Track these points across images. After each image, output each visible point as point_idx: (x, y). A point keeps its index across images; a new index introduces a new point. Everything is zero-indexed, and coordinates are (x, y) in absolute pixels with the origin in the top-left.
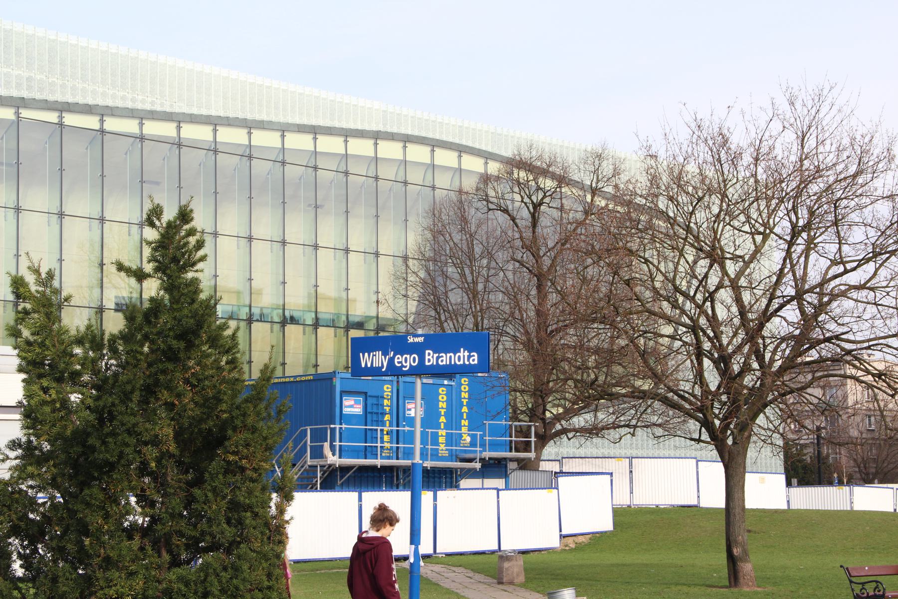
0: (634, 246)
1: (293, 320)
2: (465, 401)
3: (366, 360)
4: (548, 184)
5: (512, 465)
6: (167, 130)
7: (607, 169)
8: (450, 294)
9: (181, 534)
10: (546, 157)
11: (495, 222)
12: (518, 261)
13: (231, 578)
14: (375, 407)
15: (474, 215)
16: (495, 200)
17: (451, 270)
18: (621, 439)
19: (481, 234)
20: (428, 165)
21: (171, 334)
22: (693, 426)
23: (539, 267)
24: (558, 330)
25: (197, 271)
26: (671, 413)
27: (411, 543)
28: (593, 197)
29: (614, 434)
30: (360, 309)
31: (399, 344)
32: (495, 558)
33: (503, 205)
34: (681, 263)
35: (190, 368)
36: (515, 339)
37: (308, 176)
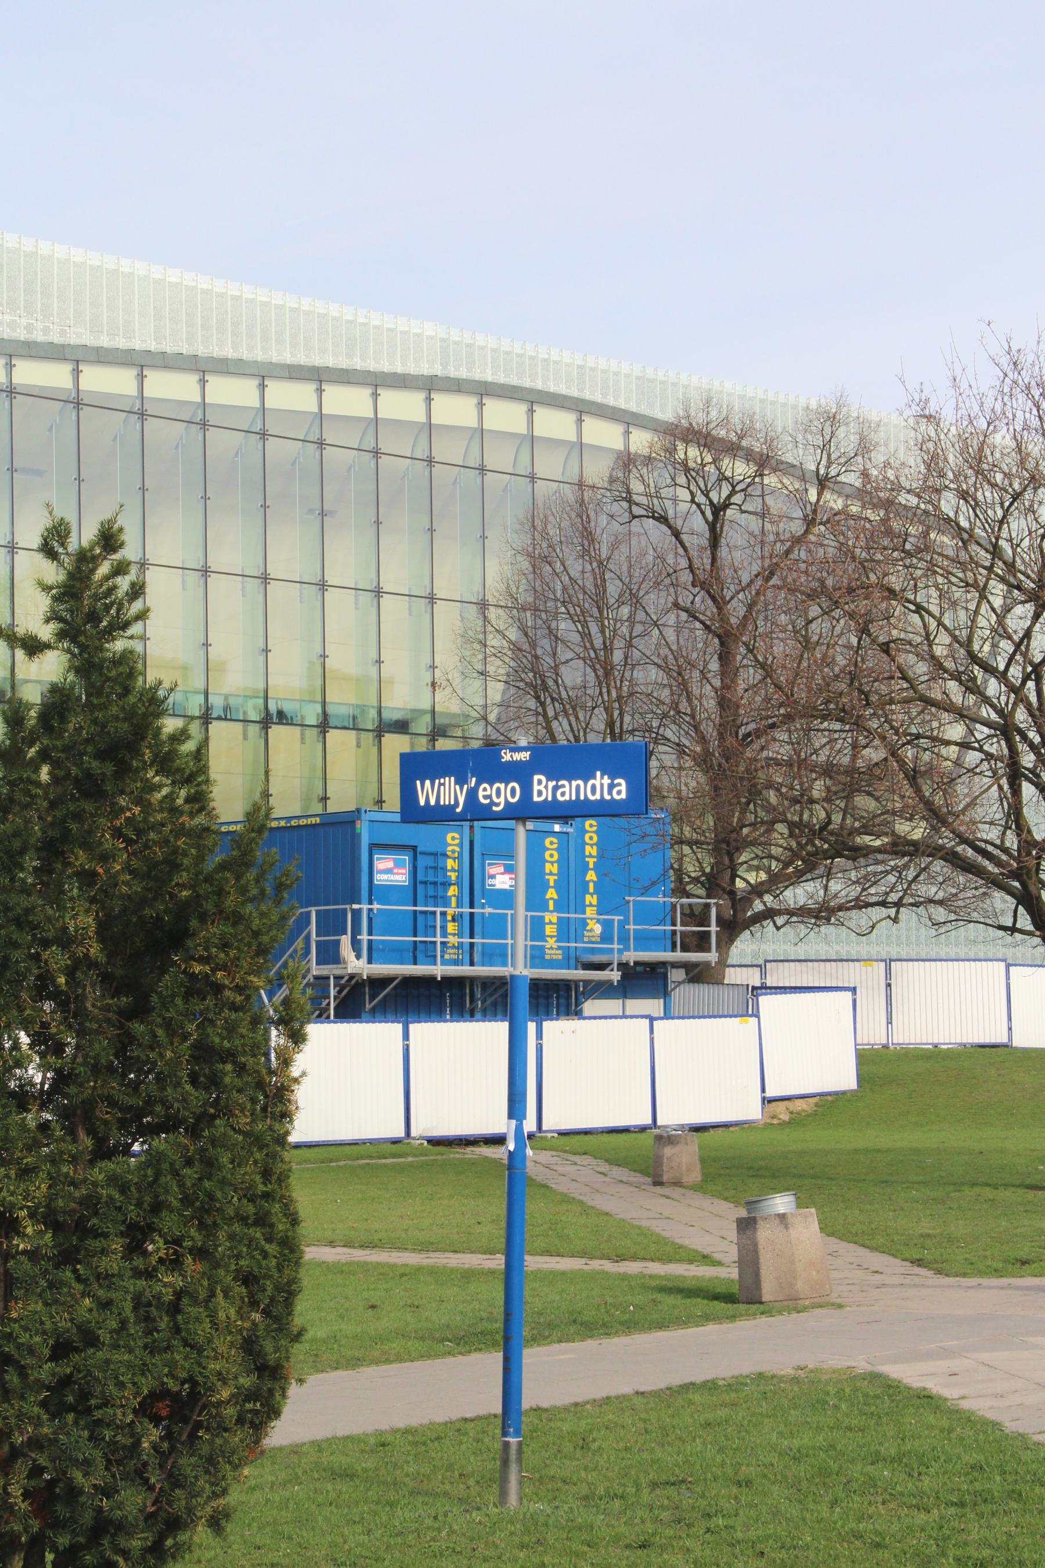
0: (895, 581)
1: (282, 717)
2: (591, 861)
3: (427, 793)
4: (741, 469)
5: (676, 975)
6: (55, 376)
7: (846, 440)
8: (563, 669)
9: (112, 1102)
10: (736, 420)
11: (643, 539)
12: (686, 610)
13: (200, 1179)
14: (431, 872)
15: (605, 528)
16: (643, 500)
17: (564, 626)
18: (873, 927)
19: (619, 562)
20: (522, 437)
21: (90, 749)
22: (1002, 903)
23: (723, 619)
24: (758, 733)
25: (132, 637)
26: (962, 879)
27: (510, 1116)
28: (820, 494)
29: (860, 918)
30: (400, 700)
31: (483, 762)
32: (647, 1139)
33: (657, 508)
34: (983, 611)
35: (122, 810)
36: (680, 750)
37: (321, 457)
